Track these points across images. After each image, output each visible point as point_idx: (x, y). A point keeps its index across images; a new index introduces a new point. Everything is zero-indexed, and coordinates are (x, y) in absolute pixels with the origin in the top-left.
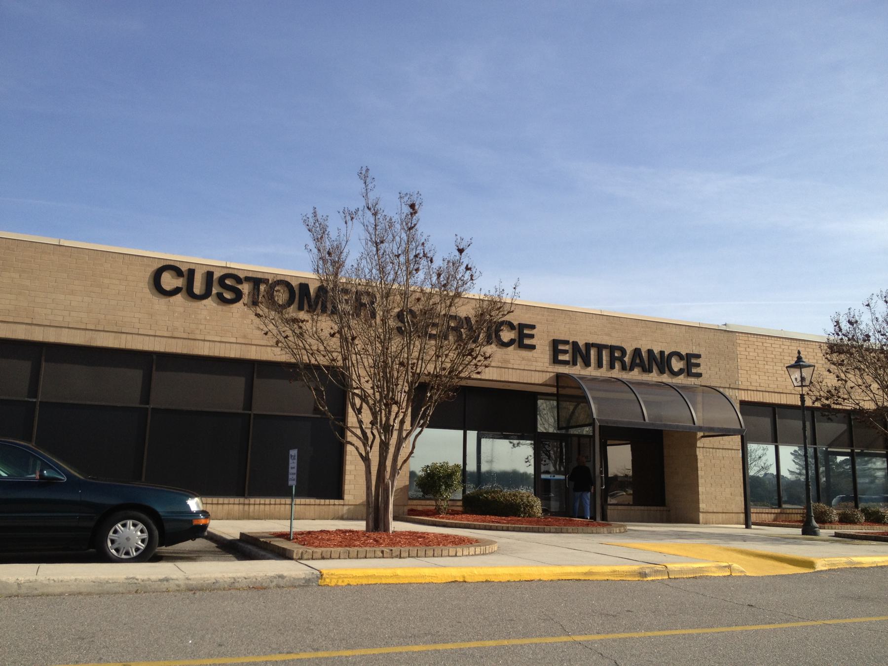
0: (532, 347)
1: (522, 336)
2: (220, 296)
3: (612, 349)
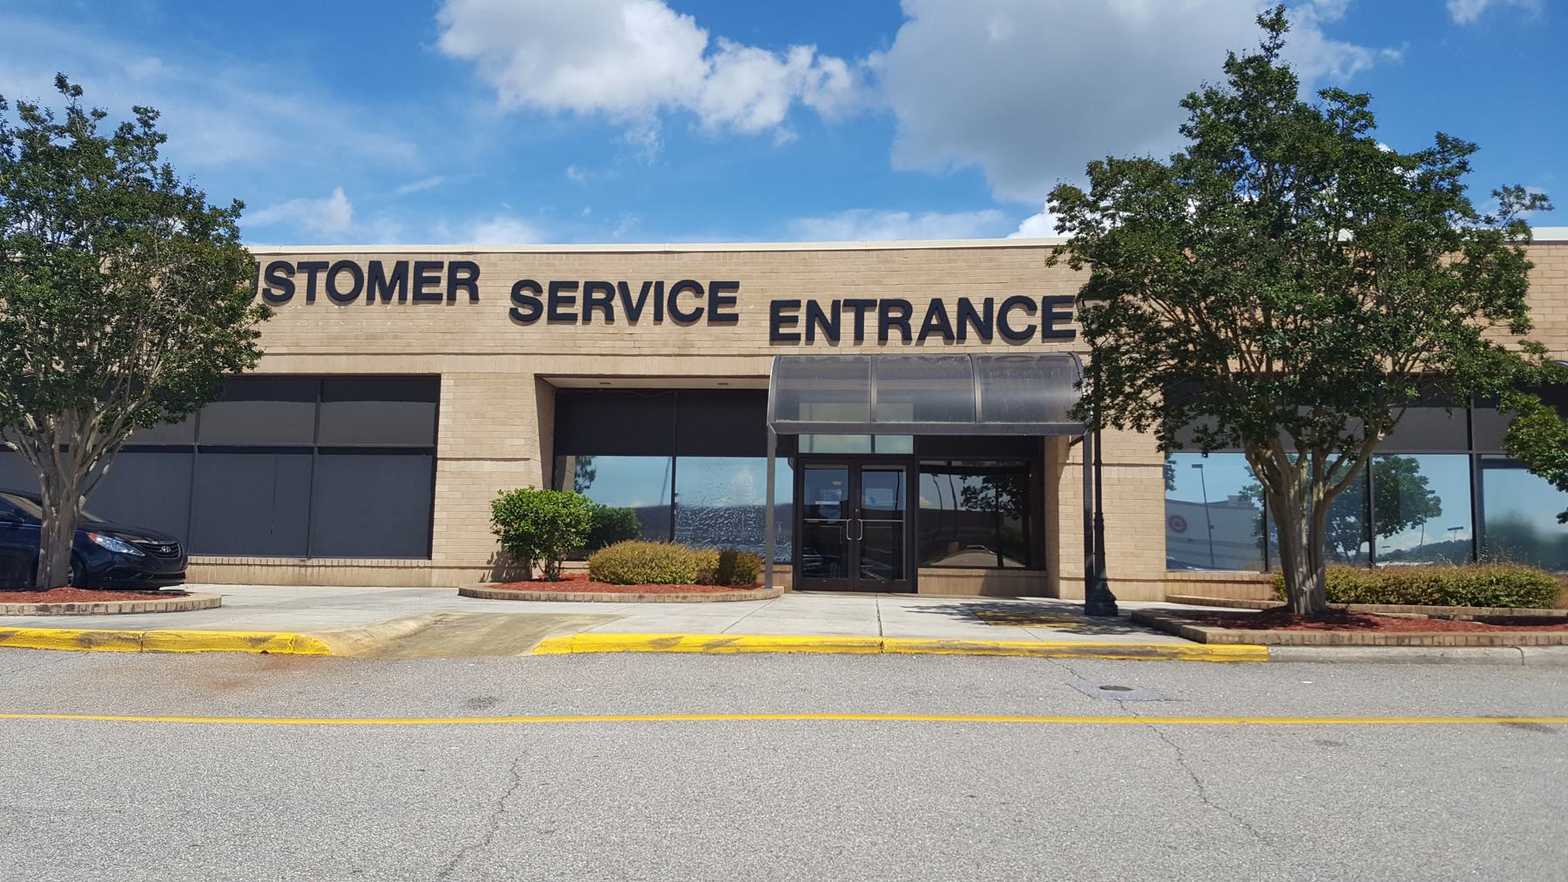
0: (732, 319)
1: (715, 302)
2: (537, 288)
3: (886, 305)
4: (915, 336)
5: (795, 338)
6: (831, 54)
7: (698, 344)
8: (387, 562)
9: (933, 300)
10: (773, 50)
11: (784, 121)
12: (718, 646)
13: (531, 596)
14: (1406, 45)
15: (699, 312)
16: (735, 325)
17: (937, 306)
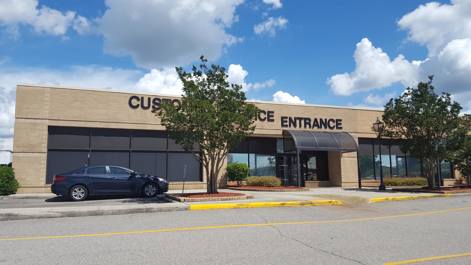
0: (273, 120)
1: (269, 116)
3: (306, 119)
4: (312, 126)
5: (287, 126)
6: (83, 15)
7: (265, 126)
8: (192, 183)
9: (315, 119)
10: (62, 11)
11: (65, 34)
12: (394, 199)
13: (276, 190)
14: (244, 37)
15: (265, 118)
16: (273, 122)
17: (316, 120)
